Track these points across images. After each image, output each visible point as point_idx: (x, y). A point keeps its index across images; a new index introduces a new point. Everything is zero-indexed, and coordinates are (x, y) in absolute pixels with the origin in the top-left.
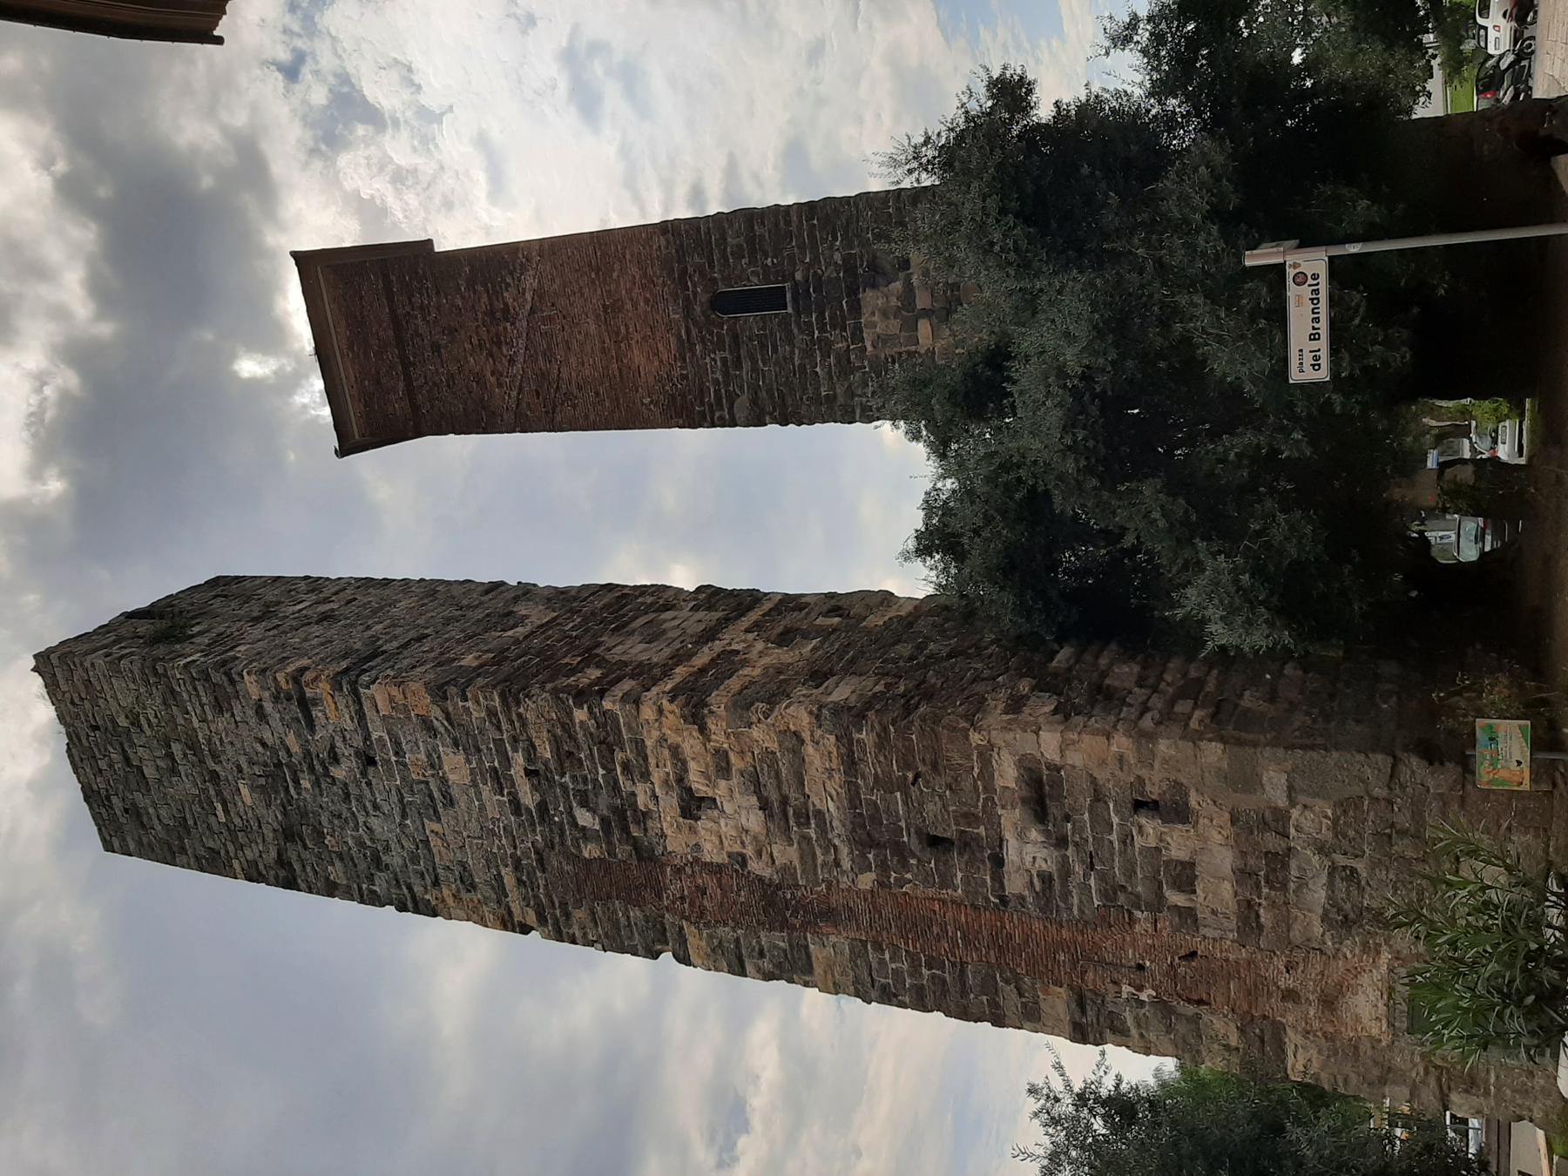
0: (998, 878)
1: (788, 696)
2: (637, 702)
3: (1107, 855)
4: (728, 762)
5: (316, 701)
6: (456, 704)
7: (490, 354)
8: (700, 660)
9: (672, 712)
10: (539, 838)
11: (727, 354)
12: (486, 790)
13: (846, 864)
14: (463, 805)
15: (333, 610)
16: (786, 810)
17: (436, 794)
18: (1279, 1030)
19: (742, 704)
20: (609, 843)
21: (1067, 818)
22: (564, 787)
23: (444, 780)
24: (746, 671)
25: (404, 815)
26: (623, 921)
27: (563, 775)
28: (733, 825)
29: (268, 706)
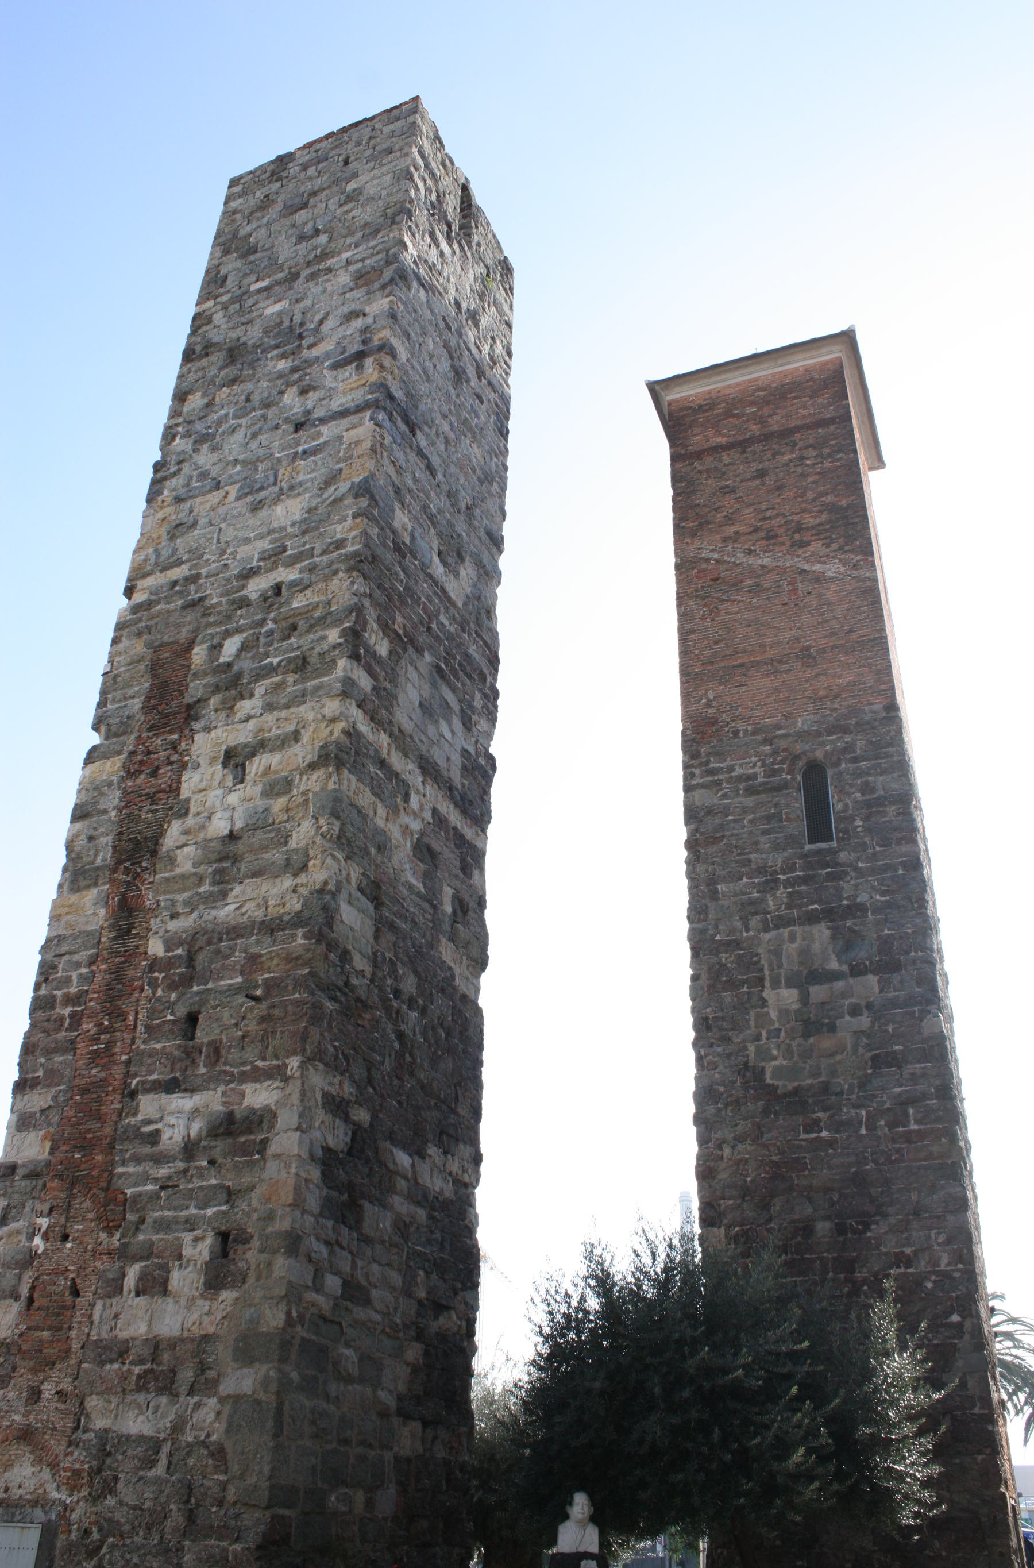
1: (348, 858)
2: (344, 694)
3: (175, 1203)
4: (279, 795)
5: (360, 368)
6: (350, 508)
7: (756, 530)
8: (396, 761)
9: (331, 733)
10: (215, 600)
12: (265, 544)
13: (173, 926)
14: (250, 522)
15: (468, 381)
16: (227, 857)
17: (263, 494)
19: (337, 807)
20: (206, 674)
21: (212, 1162)
22: (263, 622)
23: (277, 500)
24: (381, 811)
25: (245, 463)
26: (131, 692)
27: (275, 621)
28: (214, 802)
29: (358, 323)
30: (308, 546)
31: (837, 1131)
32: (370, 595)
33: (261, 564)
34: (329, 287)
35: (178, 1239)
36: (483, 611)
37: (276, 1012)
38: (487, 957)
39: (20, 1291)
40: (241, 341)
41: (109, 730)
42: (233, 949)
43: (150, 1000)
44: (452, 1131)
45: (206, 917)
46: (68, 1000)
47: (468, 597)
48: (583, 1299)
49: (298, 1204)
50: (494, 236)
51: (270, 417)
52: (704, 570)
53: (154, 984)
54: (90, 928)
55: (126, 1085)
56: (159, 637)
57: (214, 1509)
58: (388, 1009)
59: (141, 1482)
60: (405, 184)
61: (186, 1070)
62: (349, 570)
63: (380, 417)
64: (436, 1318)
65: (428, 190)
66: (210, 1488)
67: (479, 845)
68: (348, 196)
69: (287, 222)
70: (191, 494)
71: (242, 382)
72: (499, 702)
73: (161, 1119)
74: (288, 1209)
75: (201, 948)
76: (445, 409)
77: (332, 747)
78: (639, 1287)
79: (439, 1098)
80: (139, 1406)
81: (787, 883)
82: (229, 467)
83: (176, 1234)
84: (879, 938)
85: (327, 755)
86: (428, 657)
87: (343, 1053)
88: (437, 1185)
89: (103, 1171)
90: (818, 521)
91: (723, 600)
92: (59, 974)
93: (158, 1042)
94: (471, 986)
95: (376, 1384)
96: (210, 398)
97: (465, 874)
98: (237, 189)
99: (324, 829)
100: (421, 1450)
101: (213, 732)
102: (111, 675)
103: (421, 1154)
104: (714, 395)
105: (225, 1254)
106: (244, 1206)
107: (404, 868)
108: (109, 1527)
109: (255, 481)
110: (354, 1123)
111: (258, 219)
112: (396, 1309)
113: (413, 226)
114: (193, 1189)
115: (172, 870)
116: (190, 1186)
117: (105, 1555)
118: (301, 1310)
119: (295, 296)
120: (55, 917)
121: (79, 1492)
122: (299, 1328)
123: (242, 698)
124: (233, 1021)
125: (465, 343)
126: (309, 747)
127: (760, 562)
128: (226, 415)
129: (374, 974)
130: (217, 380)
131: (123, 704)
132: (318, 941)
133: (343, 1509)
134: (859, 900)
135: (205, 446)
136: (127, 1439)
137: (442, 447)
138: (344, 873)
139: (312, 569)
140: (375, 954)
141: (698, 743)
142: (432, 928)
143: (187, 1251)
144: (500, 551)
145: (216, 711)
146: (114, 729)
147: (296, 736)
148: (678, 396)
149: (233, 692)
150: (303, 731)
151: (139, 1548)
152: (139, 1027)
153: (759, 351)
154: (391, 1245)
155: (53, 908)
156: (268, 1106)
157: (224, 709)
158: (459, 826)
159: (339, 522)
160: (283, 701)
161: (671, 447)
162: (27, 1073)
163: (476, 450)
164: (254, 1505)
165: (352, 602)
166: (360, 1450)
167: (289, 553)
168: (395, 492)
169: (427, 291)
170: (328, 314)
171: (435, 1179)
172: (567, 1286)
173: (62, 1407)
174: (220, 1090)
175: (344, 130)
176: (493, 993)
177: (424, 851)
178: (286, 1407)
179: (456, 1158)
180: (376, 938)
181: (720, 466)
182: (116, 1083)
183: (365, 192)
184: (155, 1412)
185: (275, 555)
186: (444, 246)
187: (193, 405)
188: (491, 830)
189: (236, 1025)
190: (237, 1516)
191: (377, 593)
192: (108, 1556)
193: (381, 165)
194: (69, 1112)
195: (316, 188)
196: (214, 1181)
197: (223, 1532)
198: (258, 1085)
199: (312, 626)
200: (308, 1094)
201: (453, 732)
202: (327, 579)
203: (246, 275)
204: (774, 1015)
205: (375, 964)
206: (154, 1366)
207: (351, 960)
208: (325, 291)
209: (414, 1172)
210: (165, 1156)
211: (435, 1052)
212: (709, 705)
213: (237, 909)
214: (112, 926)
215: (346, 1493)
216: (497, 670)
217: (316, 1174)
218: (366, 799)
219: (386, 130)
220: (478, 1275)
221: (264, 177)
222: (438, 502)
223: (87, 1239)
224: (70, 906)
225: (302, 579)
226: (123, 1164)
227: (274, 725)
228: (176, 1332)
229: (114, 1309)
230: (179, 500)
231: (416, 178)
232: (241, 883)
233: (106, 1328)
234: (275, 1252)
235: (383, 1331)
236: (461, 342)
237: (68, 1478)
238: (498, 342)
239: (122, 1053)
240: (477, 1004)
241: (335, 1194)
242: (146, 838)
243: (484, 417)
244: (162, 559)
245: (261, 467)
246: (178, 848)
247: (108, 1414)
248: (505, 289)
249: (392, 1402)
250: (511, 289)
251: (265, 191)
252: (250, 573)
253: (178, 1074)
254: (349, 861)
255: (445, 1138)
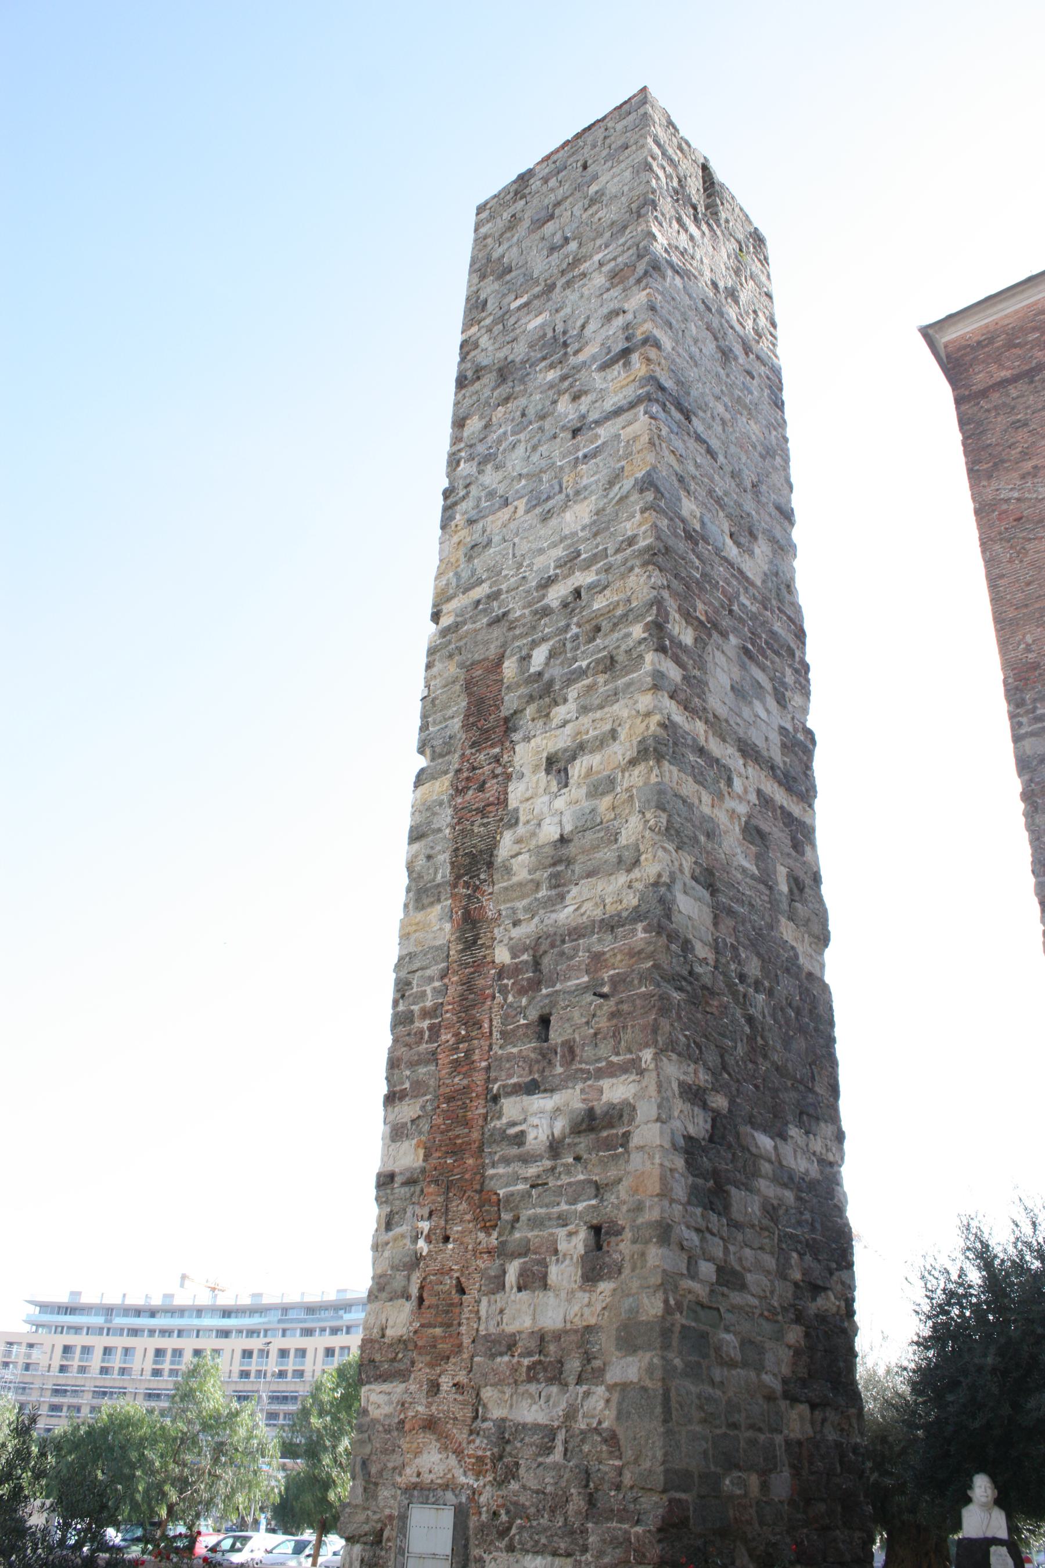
1: (678, 848)
2: (656, 687)
3: (547, 1200)
4: (603, 794)
5: (627, 364)
6: (637, 502)
8: (715, 747)
9: (648, 727)
12: (559, 552)
13: (516, 933)
14: (542, 532)
15: (736, 359)
16: (561, 861)
17: (550, 504)
18: (403, 1375)
19: (662, 800)
20: (518, 686)
21: (578, 1159)
23: (565, 507)
24: (706, 798)
26: (449, 713)
27: (579, 625)
28: (541, 809)
29: (619, 321)
30: (600, 548)
32: (669, 587)
33: (558, 571)
34: (585, 291)
35: (552, 1234)
36: (783, 587)
37: (625, 1007)
38: (829, 932)
39: (410, 1291)
40: (509, 360)
41: (434, 752)
42: (576, 949)
43: (503, 1007)
44: (811, 1111)
45: (547, 922)
46: (425, 1014)
47: (765, 574)
48: (962, 1273)
49: (665, 1194)
50: (741, 209)
51: (547, 427)
52: (1005, 512)
53: (504, 991)
54: (438, 943)
55: (488, 1090)
57: (613, 1493)
58: (734, 993)
59: (541, 1468)
60: (645, 176)
61: (543, 1071)
62: (645, 564)
63: (654, 410)
64: (814, 1299)
65: (669, 177)
66: (606, 1473)
67: (808, 821)
68: (591, 200)
69: (537, 236)
70: (481, 514)
71: (515, 399)
72: (811, 675)
73: (525, 1120)
74: (656, 1199)
75: (545, 952)
76: (717, 391)
77: (650, 741)
78: (1022, 1258)
79: (795, 1079)
80: (531, 1396)
82: (515, 483)
83: (550, 1230)
85: (646, 750)
86: (733, 640)
87: (695, 1042)
88: (802, 1166)
89: (475, 1174)
91: (1031, 539)
92: (415, 990)
93: (514, 1046)
94: (815, 964)
95: (760, 1368)
96: (487, 419)
97: (797, 852)
98: (484, 215)
99: (652, 822)
100: (811, 1433)
101: (532, 741)
102: (429, 699)
103: (783, 1136)
104: (992, 328)
105: (599, 1247)
106: (613, 1199)
107: (735, 851)
108: (516, 1510)
109: (541, 492)
110: (713, 1110)
111: (508, 239)
112: (772, 1292)
113: (660, 216)
114: (562, 1186)
115: (509, 879)
116: (559, 1183)
117: (514, 1535)
118: (678, 1297)
119: (555, 307)
120: (404, 937)
121: (485, 1477)
122: (678, 1316)
123: (556, 704)
124: (584, 1020)
125: (727, 322)
126: (628, 744)
128: (505, 433)
129: (717, 961)
130: (492, 401)
131: (443, 725)
132: (659, 933)
133: (738, 1492)
135: (489, 466)
137: (720, 429)
138: (676, 863)
139: (607, 570)
140: (716, 940)
141: (1021, 691)
142: (770, 909)
143: (562, 1246)
144: (792, 524)
145: (533, 720)
146: (438, 750)
147: (613, 734)
148: (954, 336)
149: (547, 700)
150: (619, 729)
151: (545, 1530)
152: (495, 1034)
153: (1034, 273)
154: (761, 1229)
155: (402, 927)
156: (626, 1099)
157: (540, 717)
158: (785, 804)
159: (628, 519)
160: (597, 702)
161: (953, 390)
162: (395, 1086)
163: (754, 427)
164: (651, 1489)
165: (651, 596)
166: (749, 1434)
167: (583, 556)
168: (679, 481)
169: (682, 277)
170: (588, 318)
171: (799, 1160)
172: (944, 1262)
173: (460, 1398)
174: (578, 1087)
175: (578, 136)
176: (842, 969)
177: (754, 834)
178: (673, 1393)
179: (818, 1138)
180: (716, 924)
181: (1008, 401)
182: (479, 1089)
183: (607, 192)
184: (547, 1401)
185: (570, 561)
186: (693, 229)
187: (472, 429)
188: (818, 804)
189: (587, 1023)
190: (635, 1500)
191: (675, 583)
192: (517, 1537)
193: (619, 162)
194: (438, 1120)
195: (559, 198)
196: (581, 1177)
197: (623, 1515)
198: (614, 1080)
199: (615, 625)
200: (665, 1085)
201: (767, 710)
202: (623, 577)
203: (504, 295)
205: (717, 951)
206: (542, 1358)
207: (693, 949)
208: (582, 296)
209: (778, 1155)
210: (532, 1156)
211: (786, 1033)
212: (1028, 649)
213: (576, 910)
214: (459, 939)
215: (740, 1477)
216: (804, 644)
217: (680, 1163)
218: (689, 788)
219: (619, 127)
220: (852, 1254)
221: (508, 197)
222: (722, 485)
223: (467, 1240)
224: (418, 924)
225: (599, 580)
226: (493, 1166)
227: (591, 727)
228: (559, 1325)
229: (499, 1305)
230: (471, 522)
231: (655, 168)
232: (577, 884)
233: (493, 1323)
234: (647, 1242)
235: (761, 1315)
236: (723, 321)
237: (473, 1465)
238: (760, 314)
239: (481, 1060)
240: (823, 982)
241: (700, 1181)
242: (481, 851)
243: (757, 392)
244: (463, 581)
245: (545, 477)
246: (512, 857)
247: (503, 1404)
248: (760, 260)
249: (777, 1386)
250: (766, 259)
251: (511, 211)
252: (548, 582)
253: (536, 1076)
254: (680, 852)
255: (805, 1118)
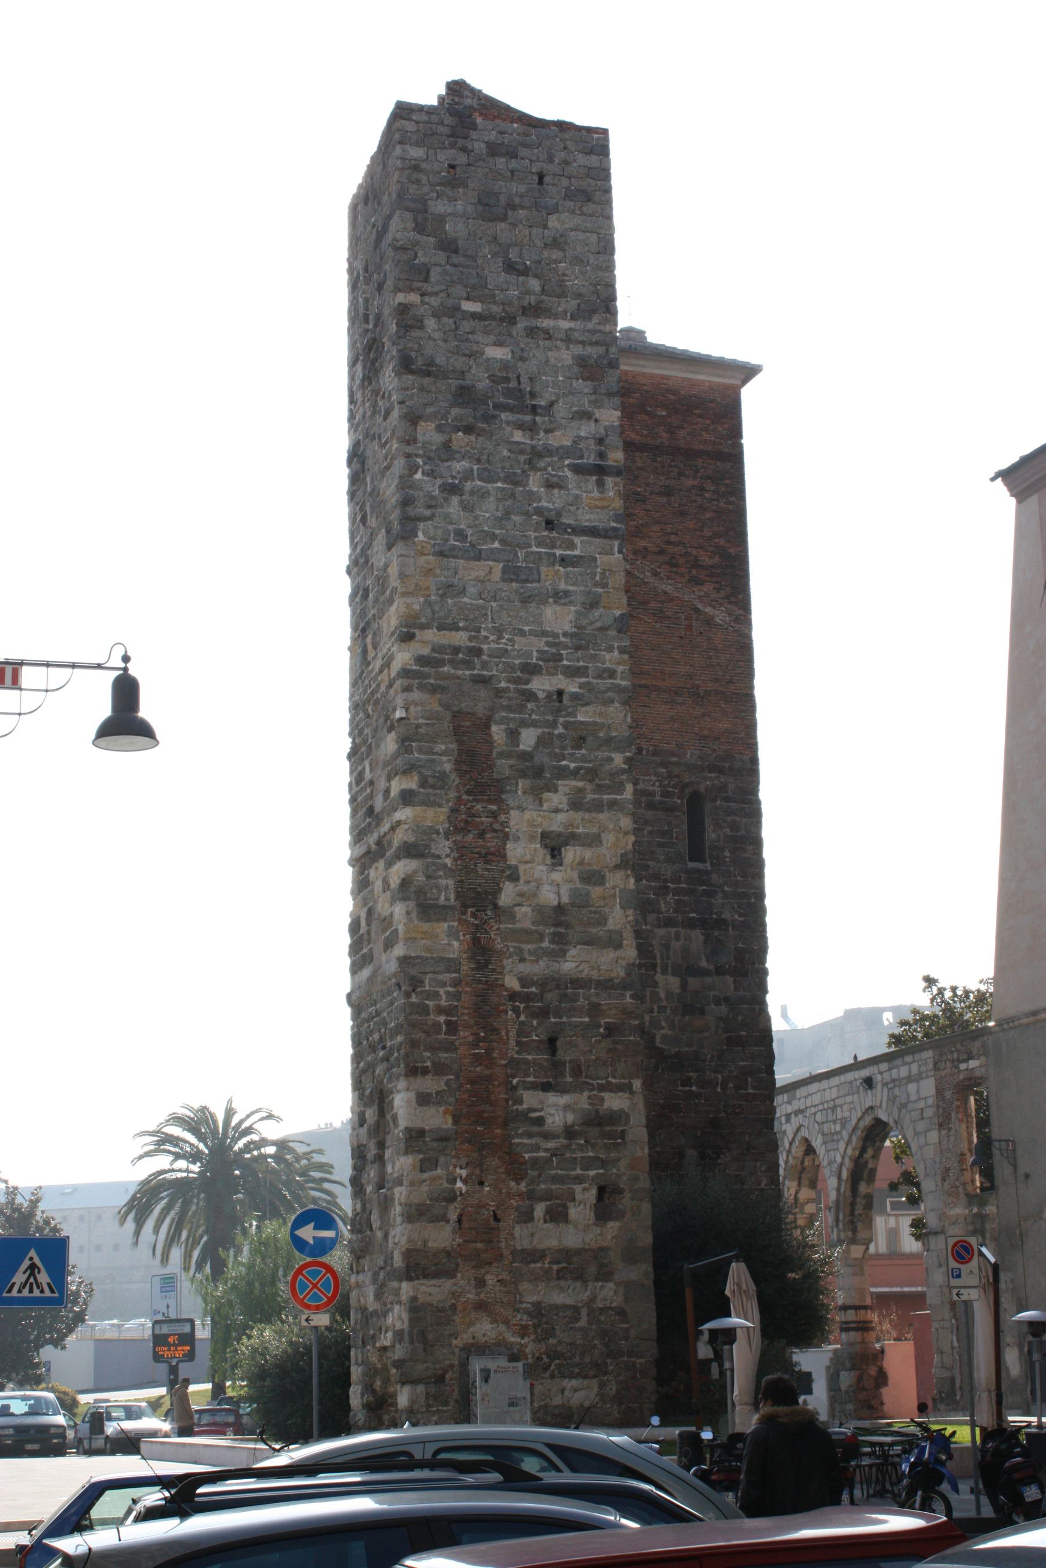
0: (534, 1086)
7: (661, 552)
11: (658, 798)
12: (541, 644)
27: (566, 726)
30: (581, 663)
31: (702, 1088)
46: (440, 1010)
56: (456, 702)
81: (676, 892)
84: (736, 949)
90: (711, 562)
127: (663, 587)
134: (723, 916)
136: (556, 1308)
143: (579, 1197)
173: (505, 1289)
196: (591, 1154)
198: (613, 1095)
204: (662, 995)
